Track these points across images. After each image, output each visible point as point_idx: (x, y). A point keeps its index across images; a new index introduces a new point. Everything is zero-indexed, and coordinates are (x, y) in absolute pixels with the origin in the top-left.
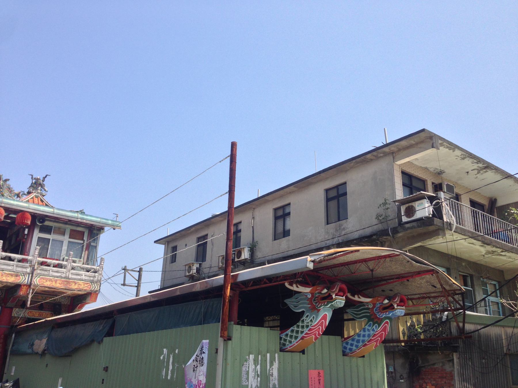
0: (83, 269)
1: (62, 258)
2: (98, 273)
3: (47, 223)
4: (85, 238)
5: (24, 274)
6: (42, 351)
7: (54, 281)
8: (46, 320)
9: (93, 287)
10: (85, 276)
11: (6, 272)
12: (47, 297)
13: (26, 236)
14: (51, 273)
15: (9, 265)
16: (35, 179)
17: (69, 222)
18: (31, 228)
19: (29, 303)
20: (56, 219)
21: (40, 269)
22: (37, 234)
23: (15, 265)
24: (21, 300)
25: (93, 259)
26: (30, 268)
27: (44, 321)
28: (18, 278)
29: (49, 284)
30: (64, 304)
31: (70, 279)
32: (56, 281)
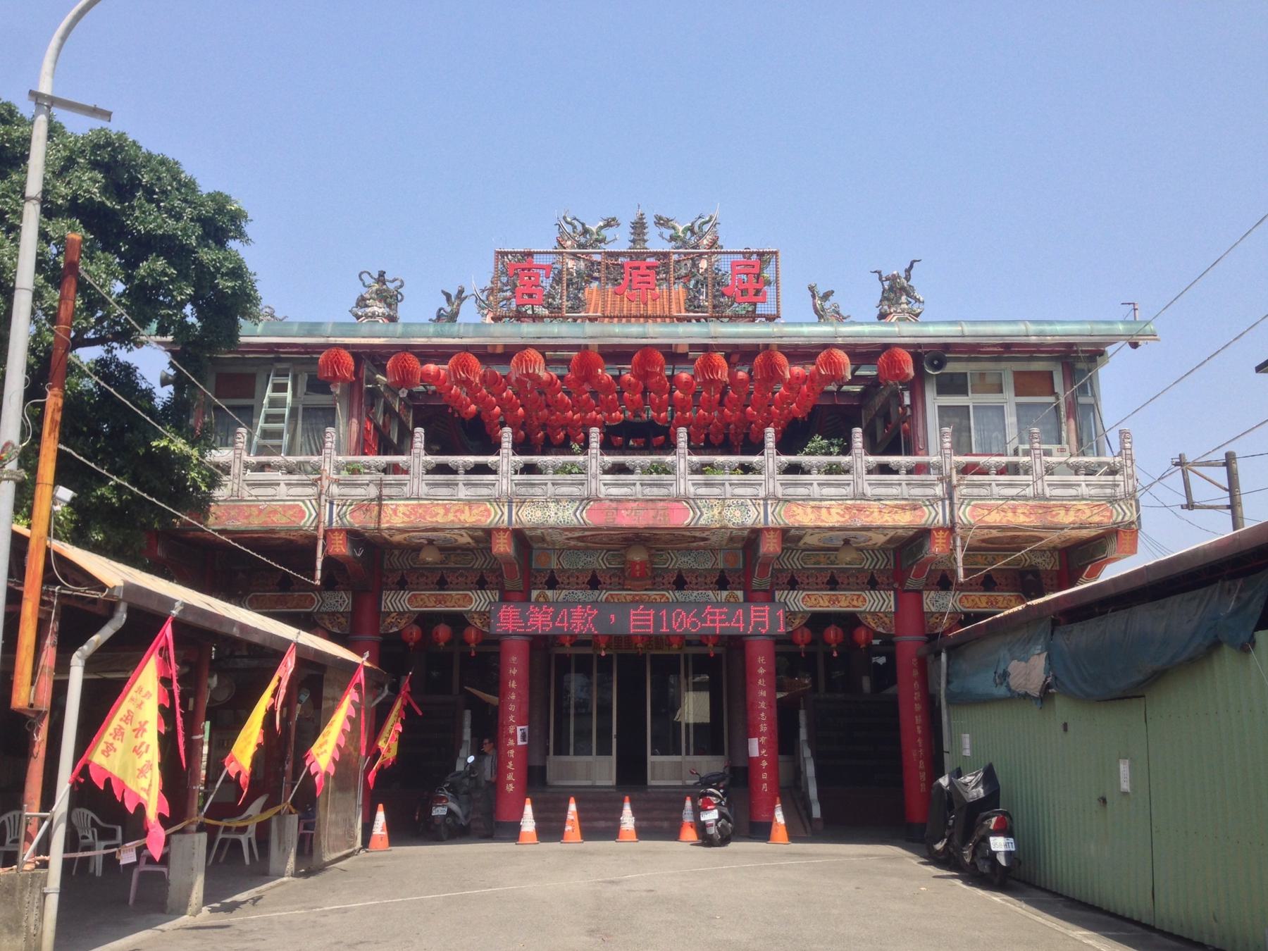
0: (1076, 470)
1: (1010, 449)
2: (1123, 474)
3: (951, 368)
4: (1059, 387)
5: (932, 501)
6: (1042, 689)
7: (1010, 511)
8: (1028, 606)
9: (1118, 514)
10: (1087, 485)
11: (888, 502)
12: (998, 555)
13: (909, 409)
14: (996, 490)
15: (890, 485)
16: (887, 279)
17: (1007, 350)
18: (916, 386)
19: (961, 572)
20: (972, 351)
21: (967, 485)
22: (934, 401)
23: (904, 483)
24: (936, 570)
25: (1094, 437)
26: (941, 485)
27: (1023, 610)
28: (918, 512)
29: (998, 520)
30: (1046, 570)
31: (1047, 499)
32: (1014, 510)
